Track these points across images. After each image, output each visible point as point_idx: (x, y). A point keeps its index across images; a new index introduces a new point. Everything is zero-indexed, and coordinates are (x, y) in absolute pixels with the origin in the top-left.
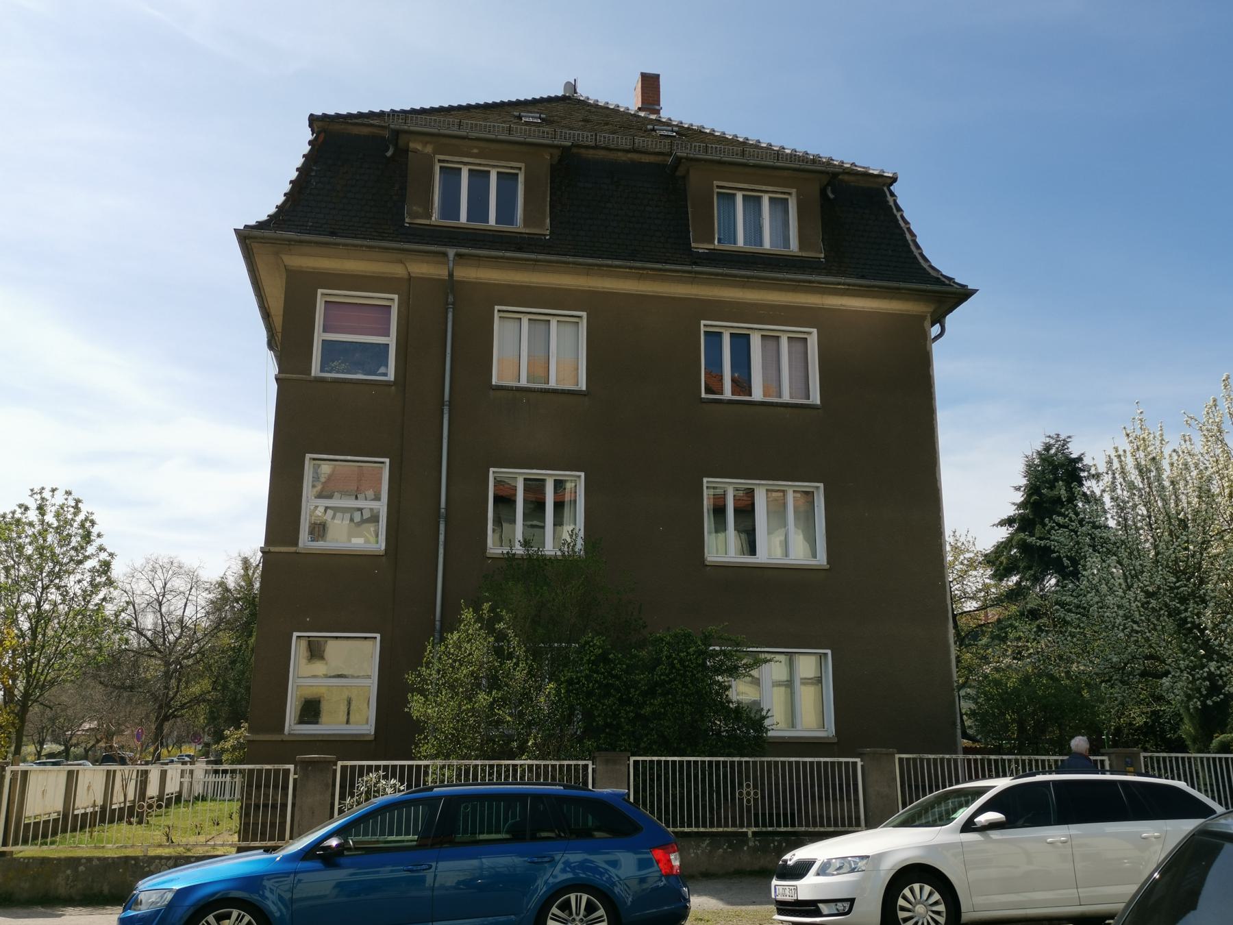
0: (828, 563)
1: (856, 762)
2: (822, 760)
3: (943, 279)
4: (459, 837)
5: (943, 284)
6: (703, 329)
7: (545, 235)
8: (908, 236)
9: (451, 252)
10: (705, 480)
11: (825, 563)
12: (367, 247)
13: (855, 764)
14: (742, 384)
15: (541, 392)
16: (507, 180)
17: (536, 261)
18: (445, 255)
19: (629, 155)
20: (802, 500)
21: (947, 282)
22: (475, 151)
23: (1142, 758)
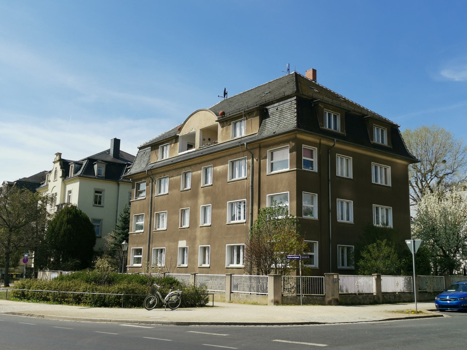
0: (354, 222)
1: (323, 278)
2: (315, 277)
3: (413, 157)
4: (210, 303)
5: (413, 158)
6: (303, 147)
7: (345, 135)
8: (404, 143)
9: (335, 140)
10: (337, 199)
11: (353, 222)
12: (321, 136)
13: (323, 278)
14: (376, 180)
15: (349, 179)
16: (335, 117)
17: (349, 144)
18: (334, 140)
19: (355, 113)
20: (347, 204)
21: (414, 158)
22: (331, 108)
23: (283, 277)
